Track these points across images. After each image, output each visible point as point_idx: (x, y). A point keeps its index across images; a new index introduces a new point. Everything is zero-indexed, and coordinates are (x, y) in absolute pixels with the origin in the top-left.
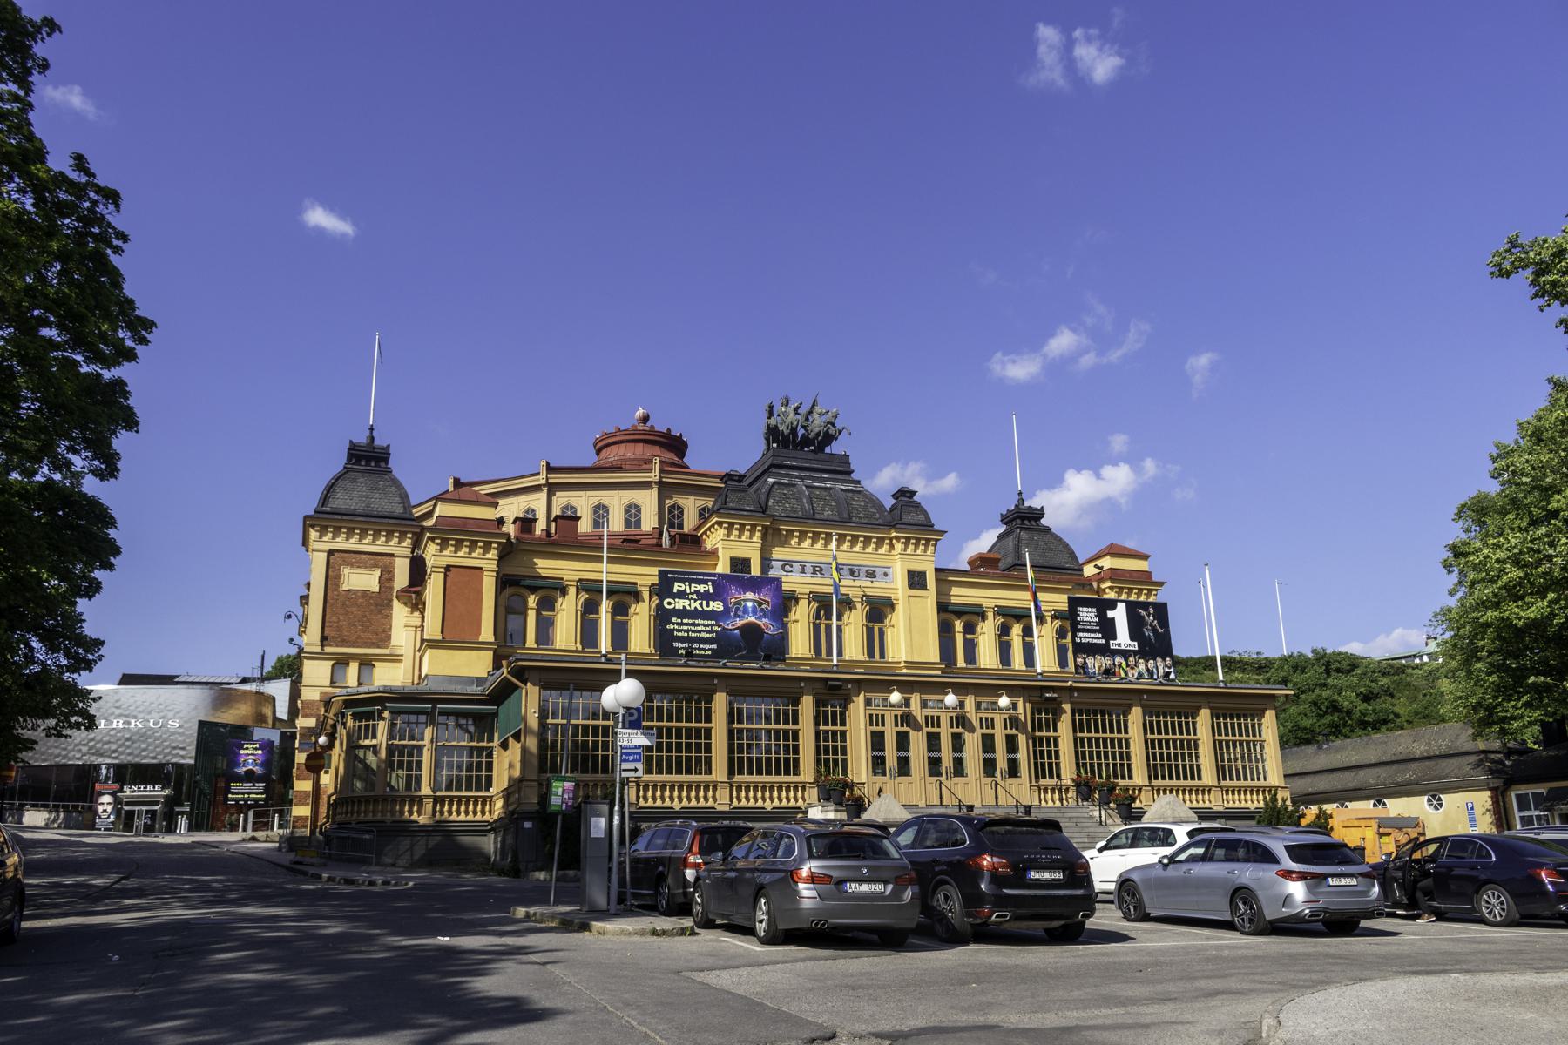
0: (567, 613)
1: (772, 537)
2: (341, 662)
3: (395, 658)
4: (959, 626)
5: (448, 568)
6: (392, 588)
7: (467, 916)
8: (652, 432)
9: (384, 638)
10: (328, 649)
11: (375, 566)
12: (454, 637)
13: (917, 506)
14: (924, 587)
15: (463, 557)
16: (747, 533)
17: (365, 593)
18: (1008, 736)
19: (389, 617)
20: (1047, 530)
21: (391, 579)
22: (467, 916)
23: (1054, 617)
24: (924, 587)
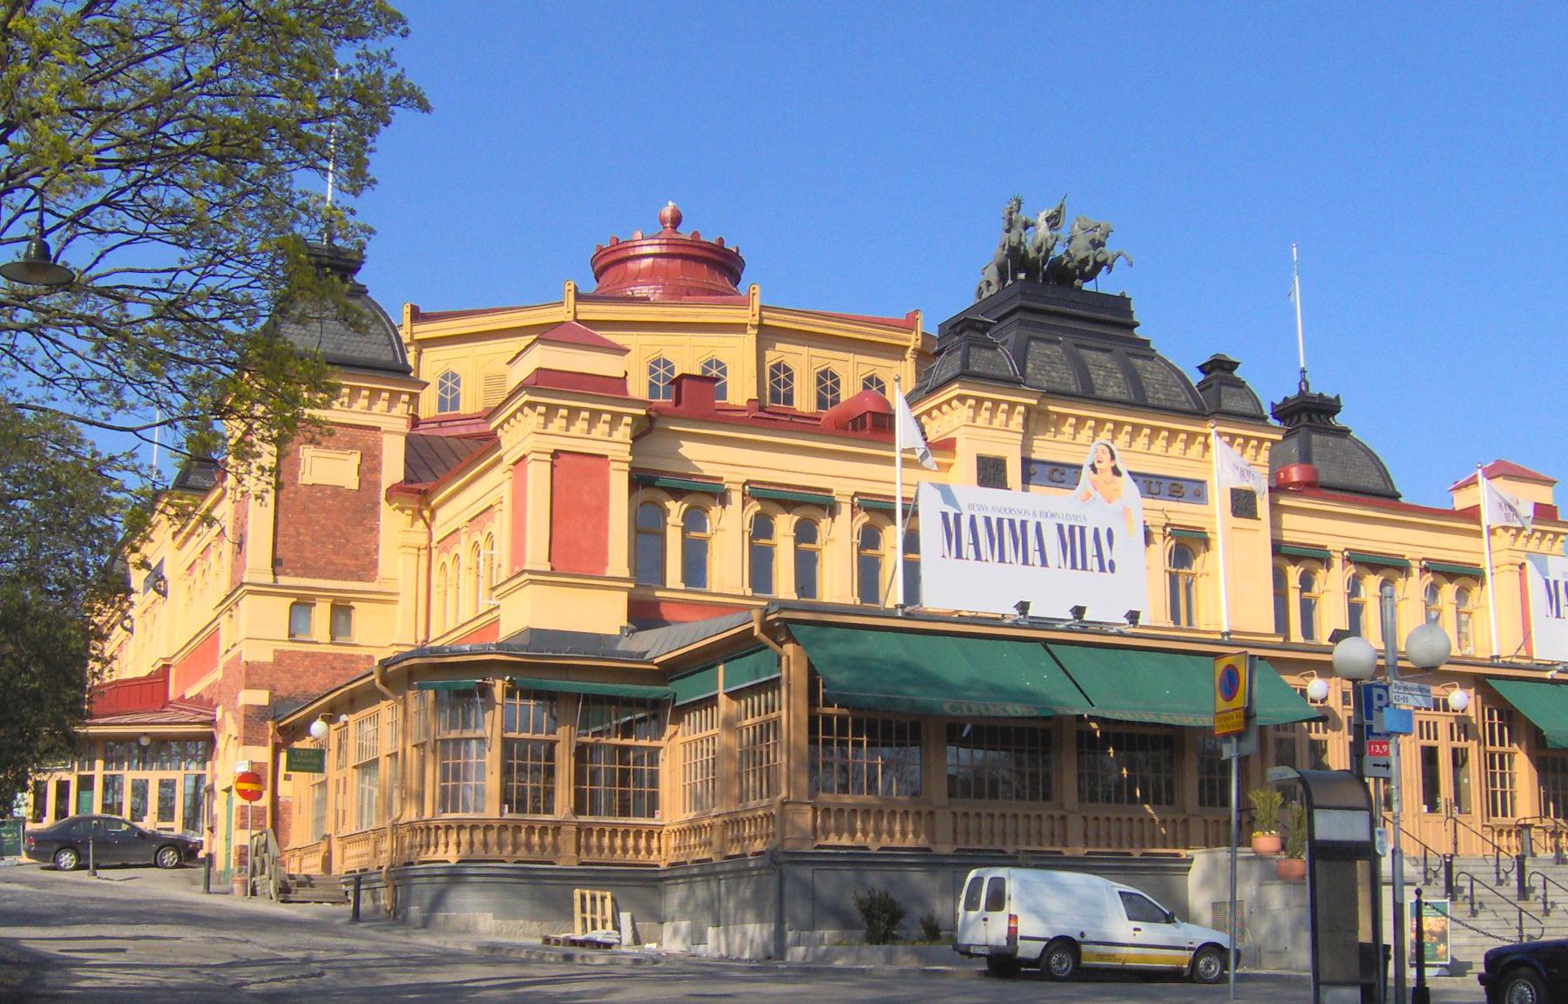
0: (728, 531)
1: (1036, 421)
2: (302, 604)
3: (387, 598)
4: (1293, 573)
5: (556, 454)
6: (377, 485)
7: (1391, 983)
8: (695, 242)
9: (366, 567)
10: (282, 580)
11: (351, 446)
12: (572, 561)
13: (1240, 384)
14: (1252, 515)
15: (579, 437)
16: (985, 415)
17: (337, 491)
18: (1455, 750)
19: (374, 530)
20: (1344, 432)
21: (376, 469)
22: (1391, 983)
23: (1424, 570)
24: (1252, 515)
